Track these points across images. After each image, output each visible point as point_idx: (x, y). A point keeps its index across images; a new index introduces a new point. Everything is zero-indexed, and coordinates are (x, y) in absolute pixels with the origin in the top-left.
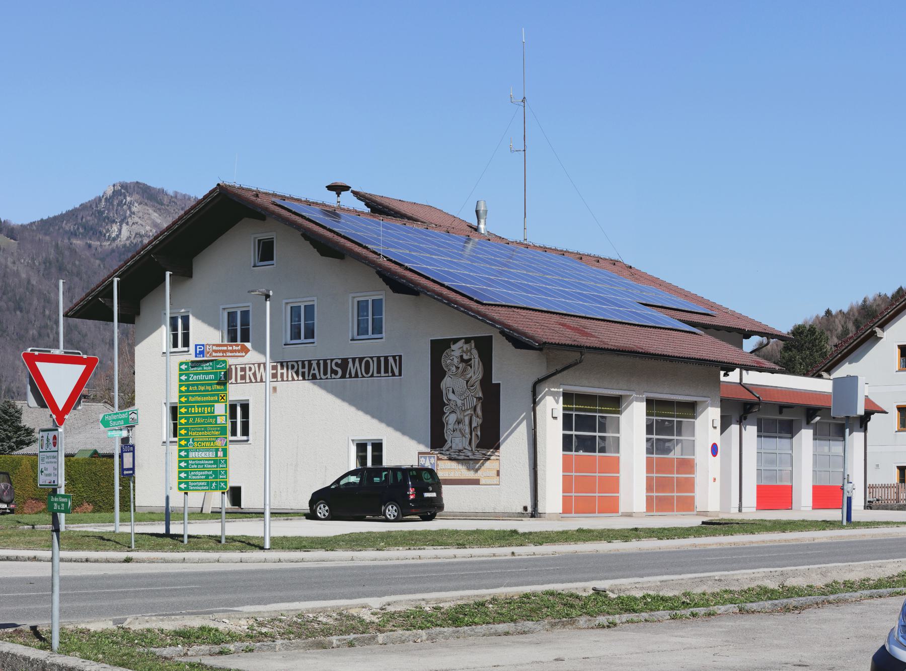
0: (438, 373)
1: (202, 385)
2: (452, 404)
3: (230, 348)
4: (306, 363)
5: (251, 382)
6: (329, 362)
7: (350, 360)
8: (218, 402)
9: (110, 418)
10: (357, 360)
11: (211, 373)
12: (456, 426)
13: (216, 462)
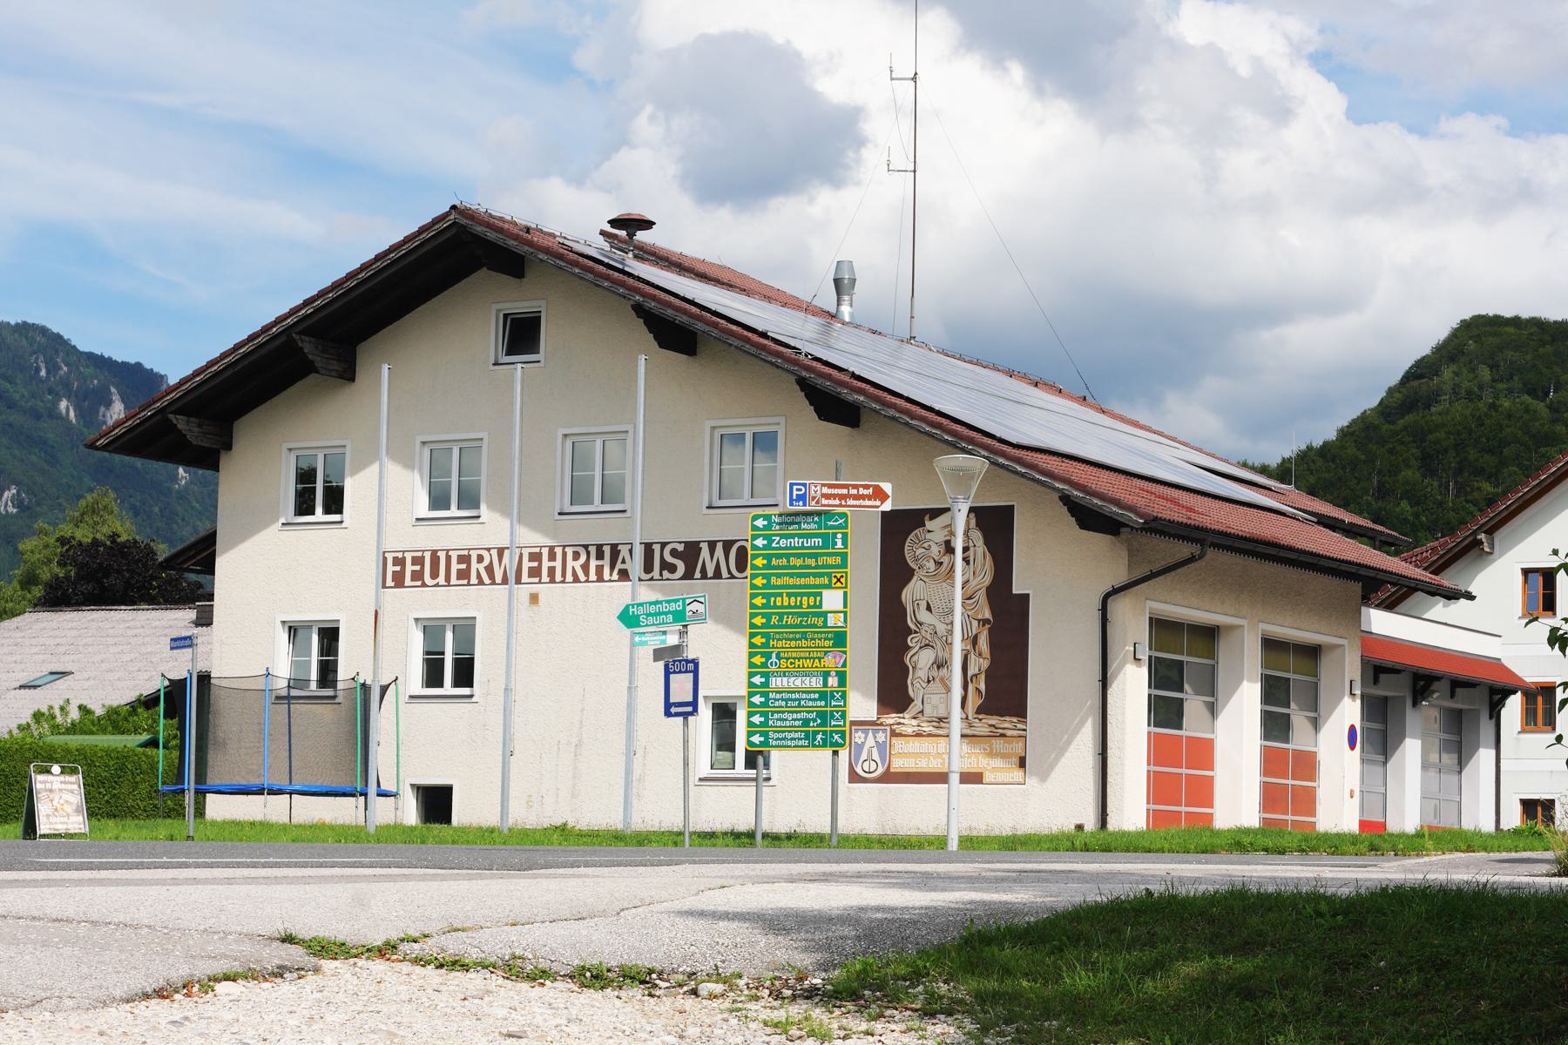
0: (895, 573)
1: (798, 556)
2: (926, 632)
3: (854, 492)
4: (607, 550)
5: (481, 582)
6: (657, 548)
7: (705, 547)
8: (829, 587)
9: (641, 610)
10: (719, 546)
11: (816, 535)
12: (934, 673)
13: (823, 696)
